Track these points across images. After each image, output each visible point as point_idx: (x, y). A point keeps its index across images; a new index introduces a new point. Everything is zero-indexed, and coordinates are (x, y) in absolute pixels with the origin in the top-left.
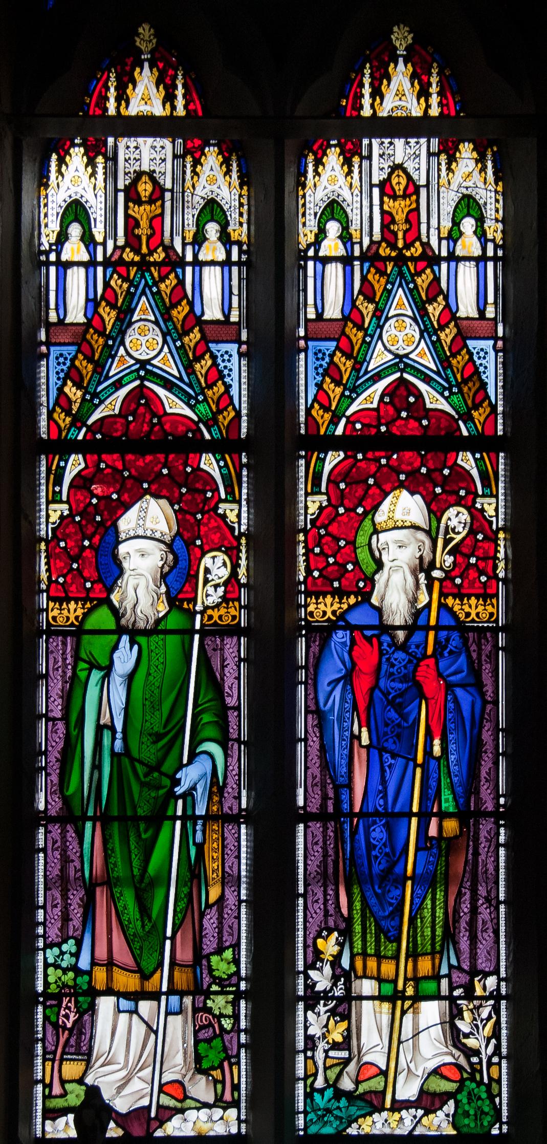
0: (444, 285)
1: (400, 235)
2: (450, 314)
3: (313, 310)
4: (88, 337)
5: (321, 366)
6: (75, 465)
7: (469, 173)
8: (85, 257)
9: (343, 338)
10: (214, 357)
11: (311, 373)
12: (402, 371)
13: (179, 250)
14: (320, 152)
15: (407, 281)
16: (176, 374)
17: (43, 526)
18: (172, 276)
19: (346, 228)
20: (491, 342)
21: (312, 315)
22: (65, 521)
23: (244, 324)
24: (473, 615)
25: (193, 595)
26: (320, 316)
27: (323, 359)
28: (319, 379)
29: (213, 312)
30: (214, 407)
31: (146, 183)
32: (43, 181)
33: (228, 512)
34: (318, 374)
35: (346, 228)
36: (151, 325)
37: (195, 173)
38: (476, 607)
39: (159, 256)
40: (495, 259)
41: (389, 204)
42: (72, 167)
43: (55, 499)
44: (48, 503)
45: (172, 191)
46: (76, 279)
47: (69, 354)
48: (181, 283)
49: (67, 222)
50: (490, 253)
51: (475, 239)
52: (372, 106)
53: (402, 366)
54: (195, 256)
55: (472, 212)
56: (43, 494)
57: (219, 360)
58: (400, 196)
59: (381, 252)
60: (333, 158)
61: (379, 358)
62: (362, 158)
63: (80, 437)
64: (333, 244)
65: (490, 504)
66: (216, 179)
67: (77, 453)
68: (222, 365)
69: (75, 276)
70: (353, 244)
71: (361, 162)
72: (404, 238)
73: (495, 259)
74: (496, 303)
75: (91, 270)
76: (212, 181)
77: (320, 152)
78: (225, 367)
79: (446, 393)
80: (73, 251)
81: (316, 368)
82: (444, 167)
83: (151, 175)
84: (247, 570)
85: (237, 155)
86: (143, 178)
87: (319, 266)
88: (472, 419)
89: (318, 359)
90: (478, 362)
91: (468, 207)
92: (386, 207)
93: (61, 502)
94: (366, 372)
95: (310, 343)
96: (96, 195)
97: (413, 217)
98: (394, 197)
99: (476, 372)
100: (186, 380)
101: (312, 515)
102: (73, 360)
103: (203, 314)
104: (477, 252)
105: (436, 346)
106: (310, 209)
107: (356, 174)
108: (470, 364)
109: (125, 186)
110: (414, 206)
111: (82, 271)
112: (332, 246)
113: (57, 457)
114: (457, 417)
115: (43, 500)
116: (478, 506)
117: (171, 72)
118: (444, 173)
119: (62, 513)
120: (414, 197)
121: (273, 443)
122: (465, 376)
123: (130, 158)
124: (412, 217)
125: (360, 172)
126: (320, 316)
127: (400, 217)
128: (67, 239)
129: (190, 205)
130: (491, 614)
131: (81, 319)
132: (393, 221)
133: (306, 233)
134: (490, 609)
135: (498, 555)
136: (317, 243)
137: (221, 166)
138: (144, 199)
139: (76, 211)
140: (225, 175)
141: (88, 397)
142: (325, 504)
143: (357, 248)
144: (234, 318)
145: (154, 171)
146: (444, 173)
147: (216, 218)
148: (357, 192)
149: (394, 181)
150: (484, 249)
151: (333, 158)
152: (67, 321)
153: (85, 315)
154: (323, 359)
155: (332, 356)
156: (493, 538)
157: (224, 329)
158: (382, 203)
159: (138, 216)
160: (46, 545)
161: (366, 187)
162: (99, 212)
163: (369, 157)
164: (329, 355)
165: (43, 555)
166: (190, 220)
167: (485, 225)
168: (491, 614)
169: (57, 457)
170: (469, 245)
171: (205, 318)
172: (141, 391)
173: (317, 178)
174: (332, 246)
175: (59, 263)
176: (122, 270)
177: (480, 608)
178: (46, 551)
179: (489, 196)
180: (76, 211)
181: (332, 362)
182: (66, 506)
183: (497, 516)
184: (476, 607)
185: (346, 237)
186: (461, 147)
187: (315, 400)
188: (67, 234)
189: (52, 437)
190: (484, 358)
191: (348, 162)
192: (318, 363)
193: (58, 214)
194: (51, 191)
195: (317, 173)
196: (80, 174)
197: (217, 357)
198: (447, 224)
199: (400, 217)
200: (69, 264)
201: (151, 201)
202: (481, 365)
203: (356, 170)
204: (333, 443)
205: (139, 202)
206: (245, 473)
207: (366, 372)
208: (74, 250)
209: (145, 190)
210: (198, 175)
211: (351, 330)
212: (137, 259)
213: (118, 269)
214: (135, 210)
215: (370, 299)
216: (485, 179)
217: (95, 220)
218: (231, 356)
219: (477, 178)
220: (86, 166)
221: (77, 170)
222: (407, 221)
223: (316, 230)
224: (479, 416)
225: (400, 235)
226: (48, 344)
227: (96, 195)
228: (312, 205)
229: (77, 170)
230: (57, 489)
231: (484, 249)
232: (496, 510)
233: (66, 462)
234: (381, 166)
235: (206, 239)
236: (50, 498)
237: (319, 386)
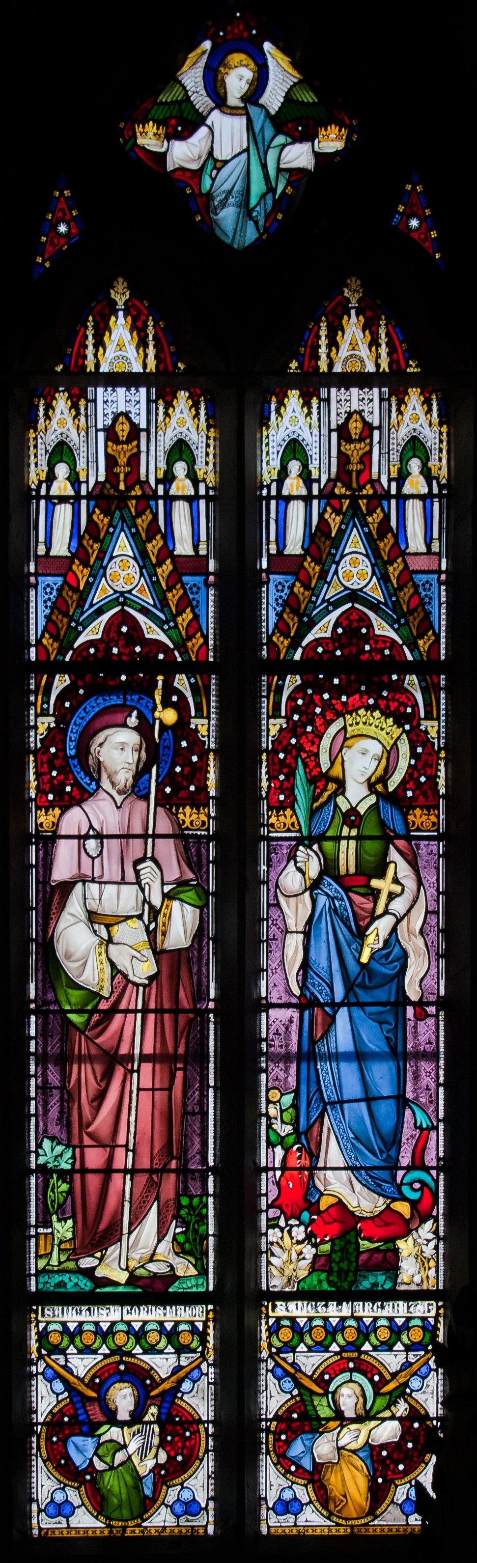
0: (393, 523)
1: (122, 476)
2: (167, 552)
3: (275, 546)
4: (306, 564)
5: (49, 599)
6: (61, 682)
7: (418, 418)
8: (304, 492)
9: (70, 573)
10: (416, 586)
11: (272, 602)
12: (123, 604)
13: (386, 486)
14: (281, 394)
15: (129, 523)
16: (151, 602)
17: (264, 739)
18: (379, 510)
19: (305, 466)
20: (436, 576)
21: (273, 551)
22: (53, 732)
23: (211, 555)
24: (187, 823)
25: (436, 803)
26: (280, 552)
27: (282, 591)
28: (279, 609)
29: (183, 547)
30: (414, 631)
31: (122, 423)
32: (264, 421)
33: (429, 729)
34: (46, 607)
35: (305, 466)
36: (361, 557)
37: (400, 412)
38: (190, 816)
39: (368, 490)
40: (440, 496)
41: (113, 448)
42: (289, 409)
43: (275, 713)
44: (269, 718)
45: (379, 428)
46: (296, 510)
47: (55, 584)
48: (387, 517)
49: (174, 459)
50: (202, 491)
51: (422, 478)
52: (96, 356)
53: (122, 599)
54: (166, 491)
55: (417, 453)
56: (264, 710)
57: (421, 590)
58: (355, 439)
59: (337, 491)
60: (61, 403)
61: (101, 593)
62: (88, 401)
63: (67, 659)
64: (63, 485)
65: (432, 727)
66: (185, 421)
67: (411, 674)
68: (424, 593)
69: (295, 508)
70: (80, 483)
71: (319, 403)
72: (125, 481)
73: (440, 496)
74: (440, 539)
75: (428, 501)
76: (294, 420)
77: (281, 394)
78: (426, 596)
79: (396, 626)
80: (60, 488)
81: (45, 602)
82: (394, 409)
83: (126, 415)
84: (446, 781)
85: (437, 396)
86: (121, 418)
87: (282, 504)
88: (417, 647)
89: (278, 591)
90: (191, 597)
91: (414, 449)
92: (109, 451)
93: (48, 715)
94: (91, 605)
95: (271, 577)
96: (311, 433)
97: (134, 460)
98: (117, 441)
99: (422, 603)
100: (159, 606)
101: (42, 734)
102: (291, 588)
103: (174, 549)
104: (425, 490)
105: (384, 578)
106: (202, 452)
107: (315, 416)
108: (416, 596)
109: (338, 425)
110: (135, 450)
111: (418, 504)
112: (61, 487)
113: (276, 677)
114: (172, 646)
115: (264, 716)
116: (423, 728)
117: (143, 318)
118: (394, 414)
119: (281, 727)
120: (368, 441)
121: (239, 667)
122: (411, 607)
123: (341, 400)
124: (365, 459)
125: (319, 413)
126: (280, 552)
127: (355, 459)
128: (287, 476)
129: (395, 441)
130: (434, 824)
131: (299, 551)
132: (116, 464)
133: (35, 474)
134: (433, 819)
135: (439, 773)
136: (280, 482)
137: (70, 410)
138: (354, 437)
139: (294, 448)
140: (194, 418)
141: (73, 624)
142: (53, 725)
143: (84, 488)
144: (203, 552)
145: (130, 412)
146: (394, 414)
147: (297, 456)
148: (83, 433)
149: (118, 428)
150: (196, 489)
151: (61, 403)
152: (286, 553)
153: (302, 547)
154: (51, 593)
155: (291, 588)
156: (204, 756)
157: (196, 564)
158: (339, 445)
159: (349, 453)
160: (267, 756)
161: (325, 431)
162: (314, 450)
163: (95, 401)
164: (289, 587)
165: (264, 764)
166: (395, 457)
167: (196, 467)
168: (204, 823)
169: (276, 677)
170: (416, 484)
171: (175, 553)
172: (124, 618)
173: (400, 417)
174: (61, 487)
175: (48, 498)
176: (335, 503)
177: (194, 817)
178: (267, 760)
179: (432, 435)
180: (294, 448)
181: (292, 592)
182: (53, 719)
183: (439, 738)
184: (190, 816)
185: (74, 480)
186: (410, 390)
187: (45, 629)
188: (54, 474)
189: (40, 659)
190: (197, 593)
191: (75, 406)
192: (279, 594)
193: (278, 452)
194: (272, 432)
195: (47, 417)
196: (297, 414)
197: (419, 586)
198: (162, 466)
199: (355, 459)
200: (289, 498)
201: (361, 439)
202: (194, 599)
203: (314, 410)
204: (62, 668)
205: (350, 440)
206: (443, 695)
207: (91, 605)
208: (293, 485)
209: (123, 430)
210: (169, 416)
211: (76, 567)
212: (348, 493)
213: (332, 501)
214: (349, 449)
215: (96, 539)
216: (198, 425)
217: (311, 456)
218: (431, 585)
219: (190, 423)
220: (302, 407)
221: (294, 411)
222: (128, 464)
223: (278, 467)
224: (423, 644)
225: (122, 476)
226: (36, 574)
227: (311, 433)
228: (395, 446)
229: (294, 411)
230: (45, 706)
231: (196, 489)
232: (438, 732)
233: (284, 681)
234: (106, 412)
235: (409, 474)
236: (39, 711)
237: (279, 615)
